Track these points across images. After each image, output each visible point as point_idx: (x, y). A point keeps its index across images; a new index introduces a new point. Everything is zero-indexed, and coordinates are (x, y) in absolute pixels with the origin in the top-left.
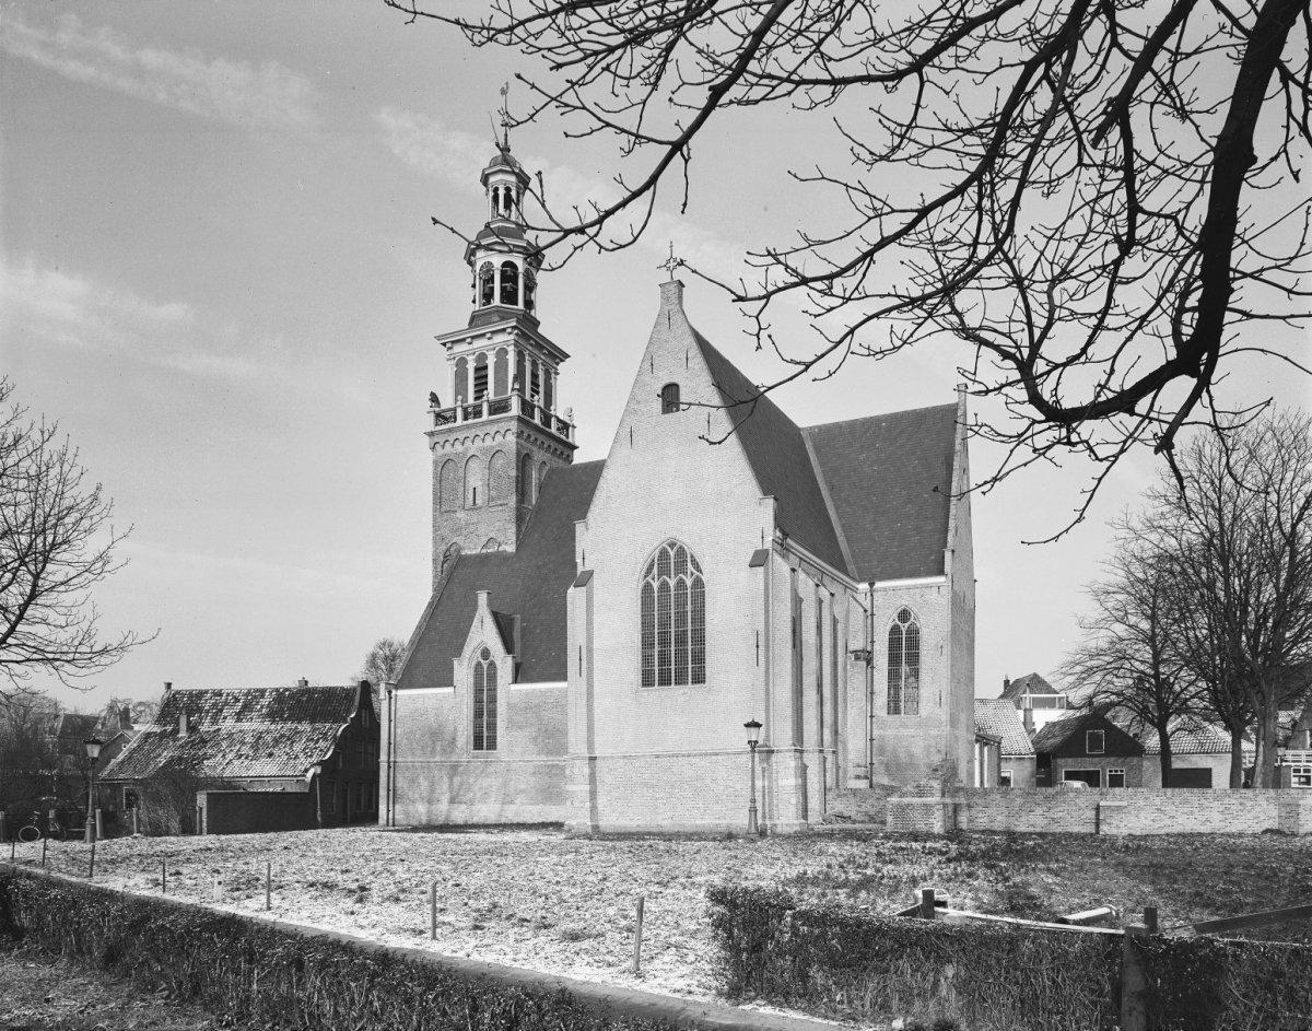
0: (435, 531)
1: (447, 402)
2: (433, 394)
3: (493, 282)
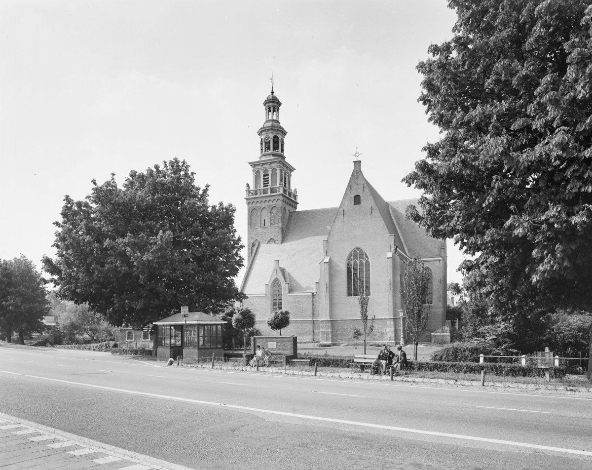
1: (252, 188)
2: (247, 184)
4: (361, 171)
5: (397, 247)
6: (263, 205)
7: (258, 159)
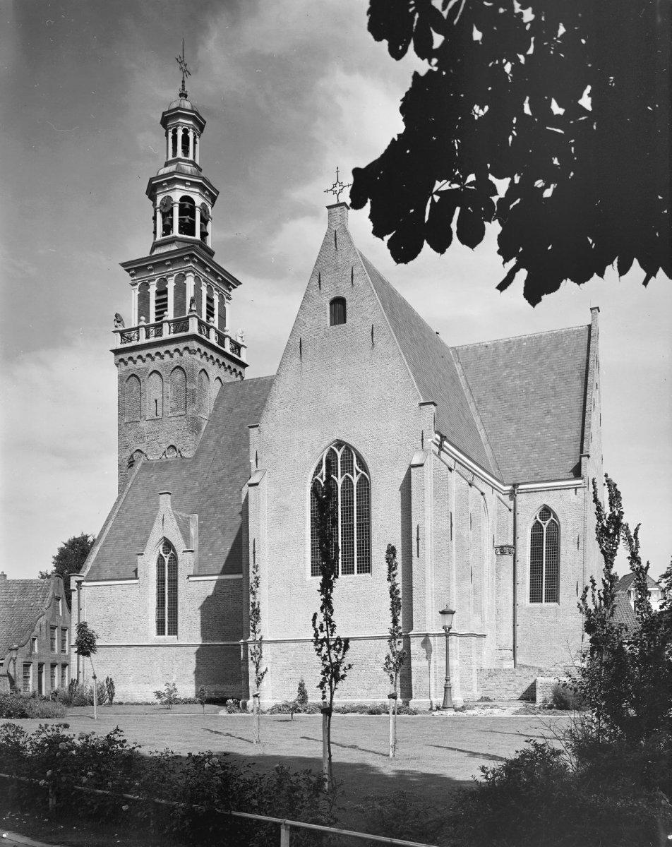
0: (120, 439)
2: (117, 315)
3: (172, 216)
4: (345, 232)
5: (443, 438)
6: (153, 365)
7: (147, 254)
